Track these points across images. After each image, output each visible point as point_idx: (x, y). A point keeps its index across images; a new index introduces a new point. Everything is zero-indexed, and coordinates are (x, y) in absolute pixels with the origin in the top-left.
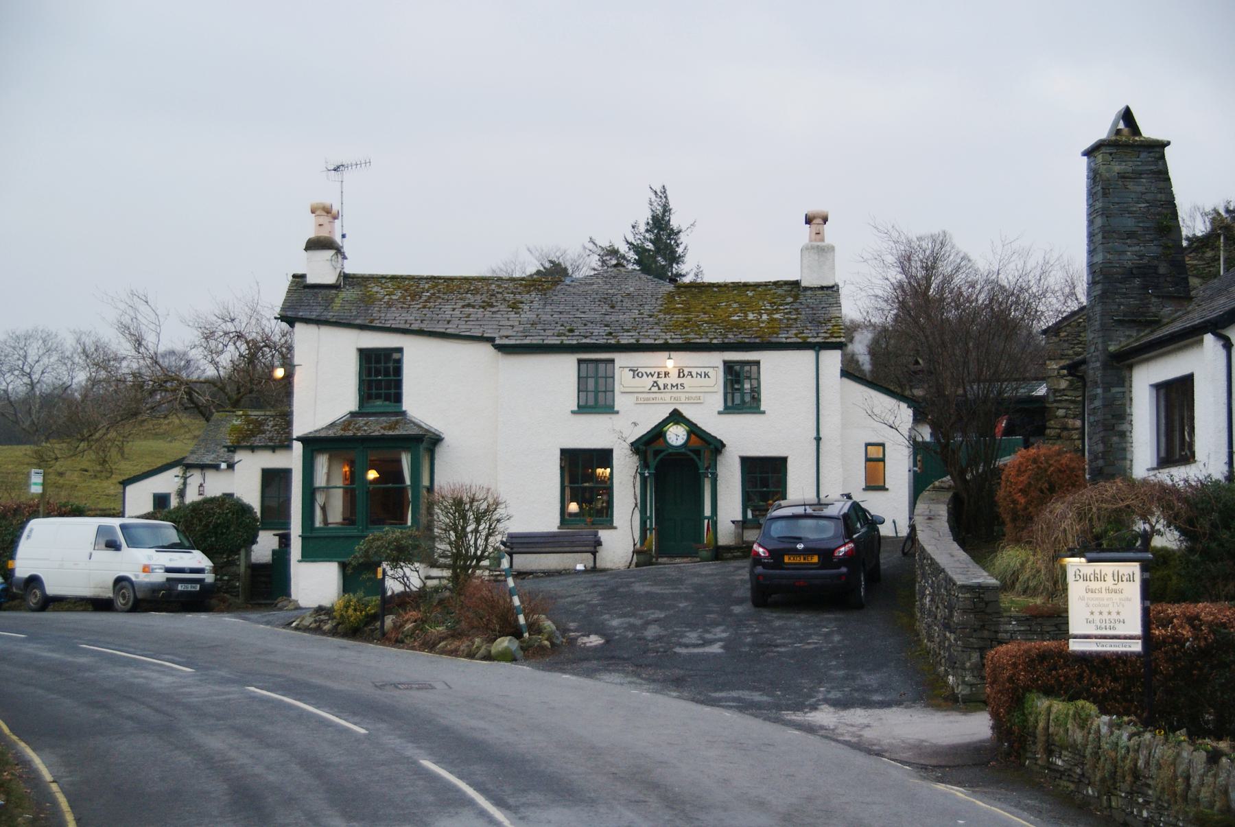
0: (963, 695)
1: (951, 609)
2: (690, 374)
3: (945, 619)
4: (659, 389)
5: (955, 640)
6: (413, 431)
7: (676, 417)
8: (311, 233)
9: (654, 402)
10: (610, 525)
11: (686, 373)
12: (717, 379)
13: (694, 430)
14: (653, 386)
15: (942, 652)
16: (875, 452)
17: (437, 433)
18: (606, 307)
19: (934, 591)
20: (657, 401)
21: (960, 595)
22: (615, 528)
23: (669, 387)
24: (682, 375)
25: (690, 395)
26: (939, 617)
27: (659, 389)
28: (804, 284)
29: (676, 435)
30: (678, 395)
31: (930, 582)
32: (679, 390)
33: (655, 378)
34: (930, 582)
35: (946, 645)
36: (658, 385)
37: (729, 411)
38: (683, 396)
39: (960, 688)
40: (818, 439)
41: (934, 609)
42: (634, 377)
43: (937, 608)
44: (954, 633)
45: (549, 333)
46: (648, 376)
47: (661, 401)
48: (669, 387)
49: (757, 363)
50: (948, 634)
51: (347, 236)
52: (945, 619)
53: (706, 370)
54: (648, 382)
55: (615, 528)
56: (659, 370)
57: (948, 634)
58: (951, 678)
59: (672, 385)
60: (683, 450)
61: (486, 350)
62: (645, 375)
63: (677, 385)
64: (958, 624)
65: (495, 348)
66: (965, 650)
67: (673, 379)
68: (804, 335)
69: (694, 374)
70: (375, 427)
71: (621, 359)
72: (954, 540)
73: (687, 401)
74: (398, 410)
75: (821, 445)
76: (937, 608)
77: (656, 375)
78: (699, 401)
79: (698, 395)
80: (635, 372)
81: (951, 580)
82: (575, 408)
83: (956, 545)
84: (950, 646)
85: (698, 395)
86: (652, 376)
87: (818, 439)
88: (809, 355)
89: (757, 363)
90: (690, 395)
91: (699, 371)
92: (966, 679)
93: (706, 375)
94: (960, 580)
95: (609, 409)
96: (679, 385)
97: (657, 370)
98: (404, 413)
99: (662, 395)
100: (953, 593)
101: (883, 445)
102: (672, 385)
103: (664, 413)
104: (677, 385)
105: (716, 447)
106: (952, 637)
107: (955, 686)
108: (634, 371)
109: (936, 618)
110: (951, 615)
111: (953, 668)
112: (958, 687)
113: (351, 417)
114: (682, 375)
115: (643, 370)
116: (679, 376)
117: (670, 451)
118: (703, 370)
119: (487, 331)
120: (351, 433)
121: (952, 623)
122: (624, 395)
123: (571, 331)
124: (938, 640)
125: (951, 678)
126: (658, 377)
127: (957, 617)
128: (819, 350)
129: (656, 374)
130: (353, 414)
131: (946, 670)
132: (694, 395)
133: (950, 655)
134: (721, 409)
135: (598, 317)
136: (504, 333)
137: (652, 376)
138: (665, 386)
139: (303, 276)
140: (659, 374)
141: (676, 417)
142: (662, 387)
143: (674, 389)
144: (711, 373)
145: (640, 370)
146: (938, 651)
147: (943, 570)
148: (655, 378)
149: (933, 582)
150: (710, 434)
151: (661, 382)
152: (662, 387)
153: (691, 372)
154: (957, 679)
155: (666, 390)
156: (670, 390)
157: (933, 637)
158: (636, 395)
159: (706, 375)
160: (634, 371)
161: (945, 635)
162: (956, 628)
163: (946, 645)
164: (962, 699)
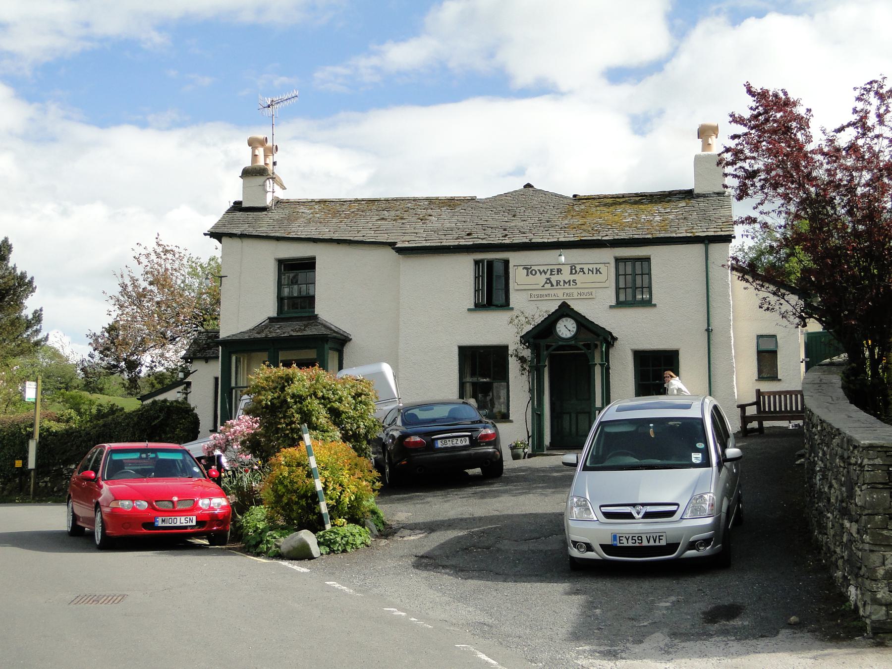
0: (873, 622)
1: (851, 485)
2: (582, 270)
3: (842, 501)
4: (552, 285)
5: (858, 532)
6: (324, 331)
7: (564, 311)
8: (248, 163)
9: (548, 298)
10: (505, 417)
11: (578, 270)
12: (609, 273)
13: (583, 323)
14: (546, 283)
15: (838, 550)
16: (768, 346)
17: (345, 334)
18: (510, 217)
19: (825, 465)
20: (550, 298)
21: (866, 461)
22: (511, 421)
23: (562, 283)
24: (574, 271)
25: (582, 291)
26: (833, 500)
27: (552, 285)
28: (696, 192)
29: (566, 329)
30: (571, 291)
31: (820, 455)
32: (572, 286)
33: (548, 276)
34: (820, 455)
35: (845, 540)
36: (551, 282)
37: (619, 306)
38: (575, 292)
39: (869, 608)
40: (709, 331)
41: (826, 489)
42: (527, 275)
43: (831, 487)
44: (857, 521)
45: (448, 237)
46: (541, 273)
47: (554, 298)
48: (562, 283)
49: (647, 259)
50: (847, 524)
51: (277, 163)
52: (842, 501)
53: (598, 266)
54: (542, 279)
55: (511, 421)
56: (552, 267)
57: (847, 524)
58: (852, 589)
59: (564, 281)
60: (573, 342)
61: (390, 253)
62: (538, 272)
63: (569, 281)
64: (863, 508)
65: (397, 252)
66: (875, 548)
67: (566, 275)
68: (694, 231)
69: (586, 271)
70: (289, 330)
71: (515, 259)
72: (851, 403)
73: (579, 297)
74: (311, 314)
75: (711, 336)
76: (831, 487)
77: (549, 272)
78: (591, 297)
79: (590, 290)
80: (528, 270)
81: (850, 441)
82: (472, 307)
83: (853, 407)
84: (851, 541)
85: (590, 290)
86: (545, 273)
87: (709, 331)
88: (699, 248)
89: (647, 259)
90: (582, 291)
91: (591, 267)
92: (879, 596)
93: (598, 271)
94: (865, 441)
95: (505, 305)
96: (571, 281)
97: (550, 267)
98: (316, 317)
99: (555, 292)
100: (853, 460)
101: (774, 336)
102: (564, 281)
103: (553, 307)
104: (569, 281)
105: (608, 339)
106: (854, 528)
107: (860, 604)
108: (527, 269)
109: (829, 500)
110: (851, 495)
111: (857, 576)
112: (864, 605)
113: (270, 322)
114: (574, 271)
115: (536, 268)
116: (571, 273)
117: (560, 343)
118: (595, 266)
119: (390, 237)
120: (263, 335)
121: (852, 507)
122: (518, 292)
123: (469, 235)
124: (832, 532)
125: (852, 589)
126: (551, 274)
127: (861, 497)
128: (708, 244)
129: (549, 271)
130: (271, 320)
131: (845, 577)
132: (586, 291)
133: (850, 555)
134: (614, 303)
135: (498, 224)
136: (407, 238)
137: (545, 273)
138: (558, 283)
139: (240, 203)
140: (551, 271)
141: (564, 311)
142: (555, 284)
143: (567, 286)
144: (603, 269)
145: (533, 268)
146: (832, 547)
147: (839, 432)
148: (548, 276)
149: (824, 454)
150: (580, 314)
151: (554, 279)
152: (555, 284)
153: (582, 269)
154: (862, 594)
155: (559, 287)
156: (562, 287)
157: (826, 528)
158: (530, 292)
159: (598, 271)
160: (527, 269)
161: (842, 525)
162: (860, 515)
163: (845, 540)
164: (873, 629)
